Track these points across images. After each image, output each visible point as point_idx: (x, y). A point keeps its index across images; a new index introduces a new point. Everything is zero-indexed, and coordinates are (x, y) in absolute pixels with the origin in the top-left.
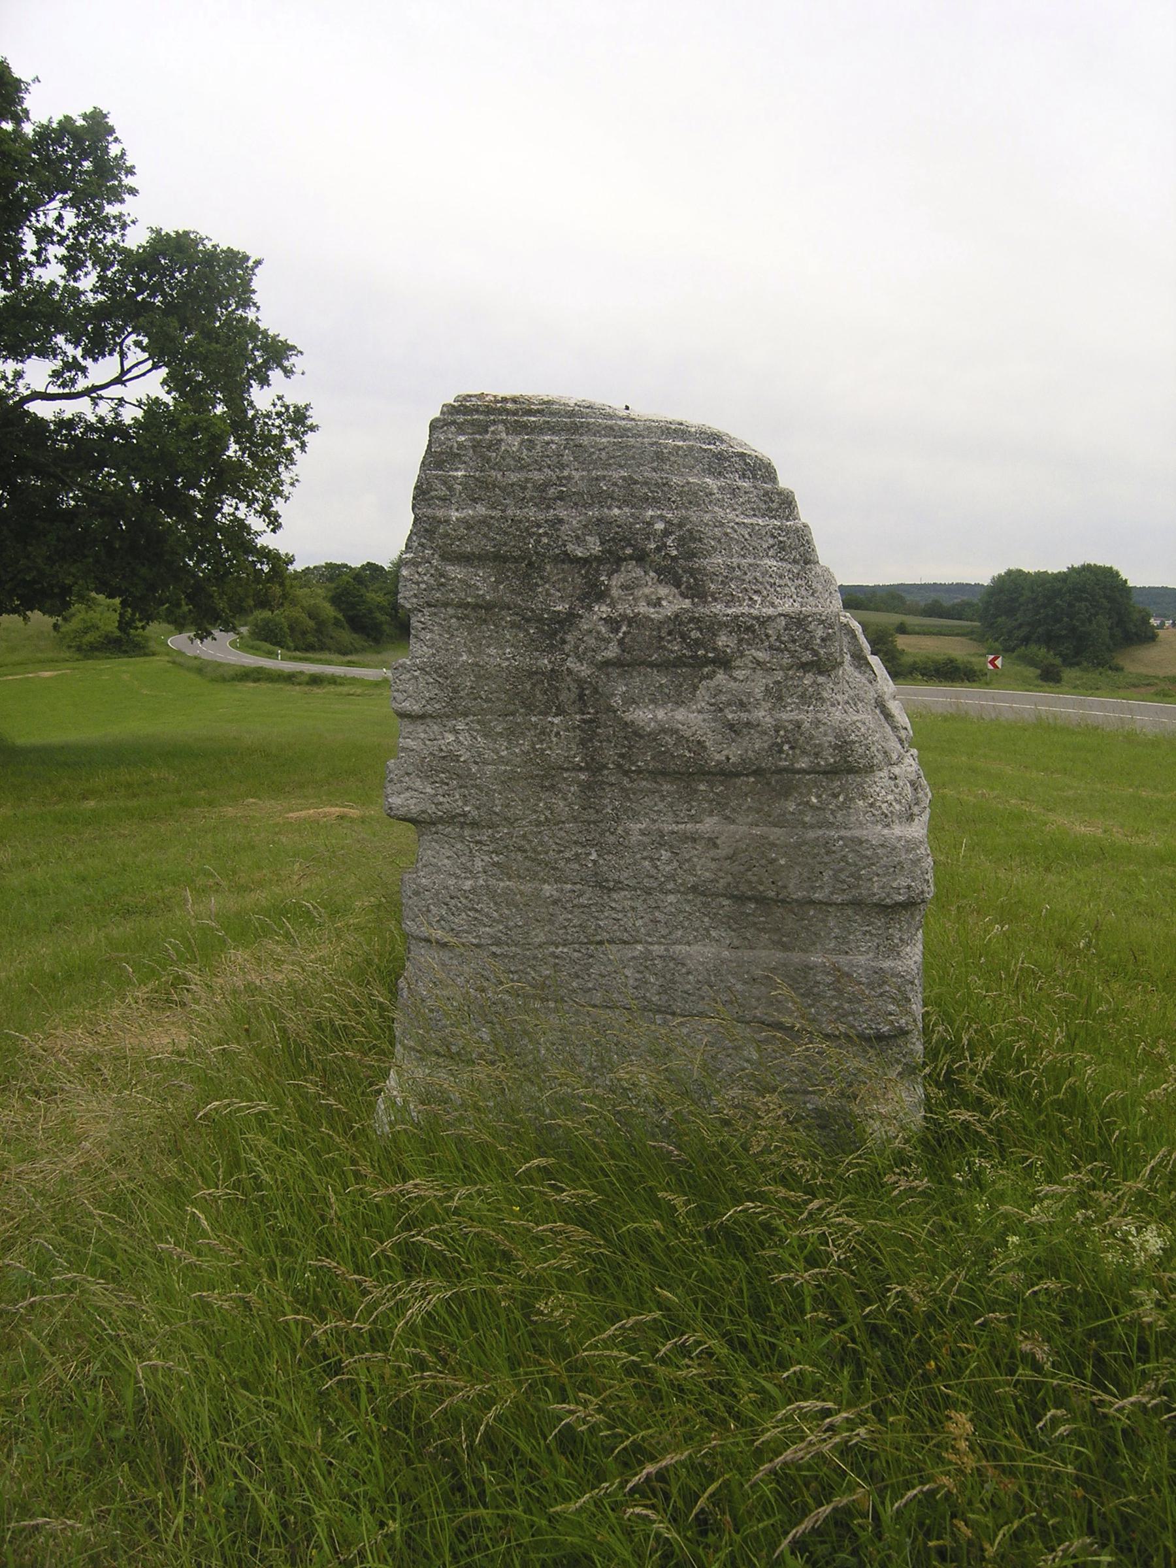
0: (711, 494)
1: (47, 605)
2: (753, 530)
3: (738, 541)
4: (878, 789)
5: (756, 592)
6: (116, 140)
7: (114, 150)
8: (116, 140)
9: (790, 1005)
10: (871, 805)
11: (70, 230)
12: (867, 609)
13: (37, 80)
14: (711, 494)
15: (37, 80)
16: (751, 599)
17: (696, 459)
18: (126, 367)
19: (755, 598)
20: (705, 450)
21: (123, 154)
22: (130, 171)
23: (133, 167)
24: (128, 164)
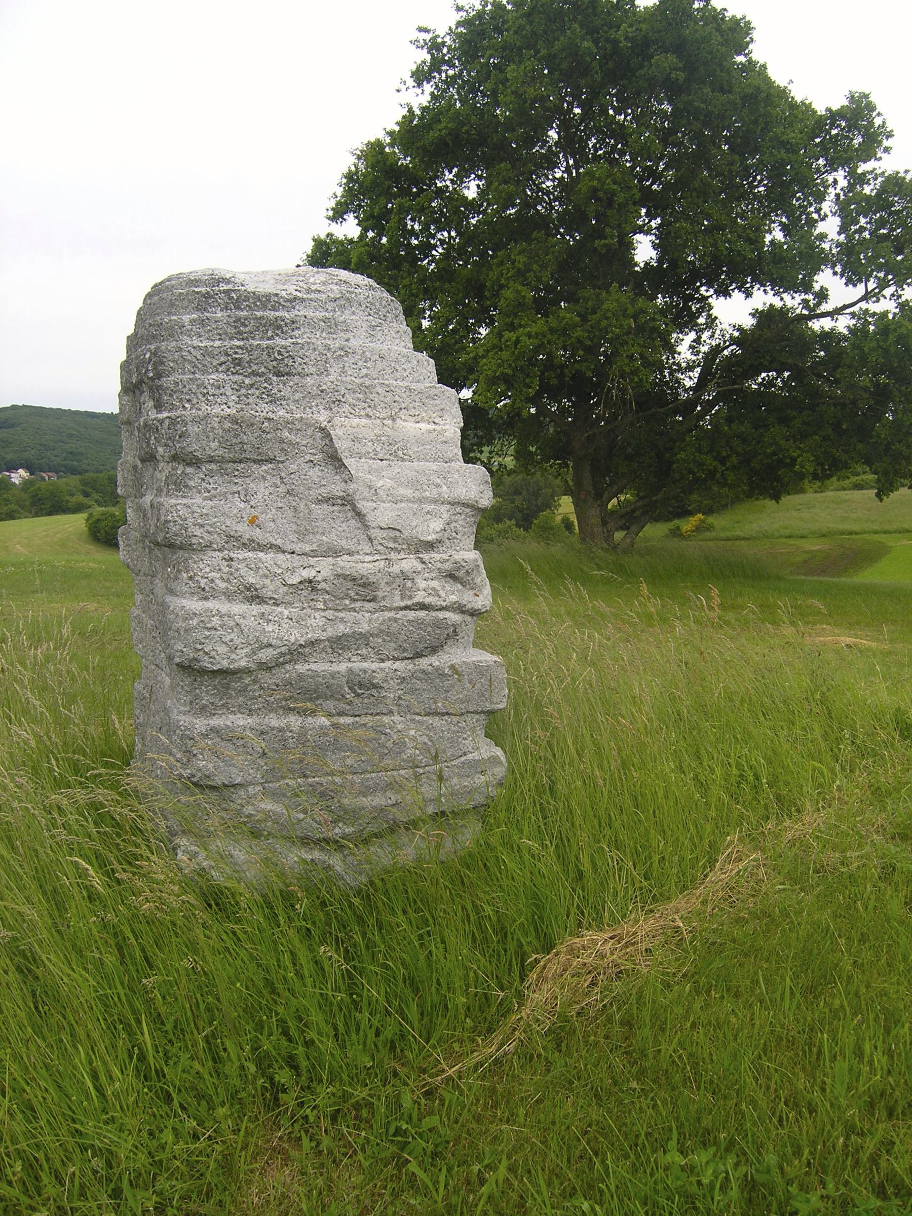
0: (184, 326)
1: (126, 398)
2: (206, 352)
3: (190, 362)
4: (202, 566)
5: (189, 401)
6: (879, 114)
7: (878, 122)
8: (879, 114)
9: (841, 898)
10: (191, 578)
11: (842, 189)
12: (867, 489)
13: (791, 81)
14: (184, 326)
15: (791, 81)
16: (184, 406)
17: (189, 301)
18: (869, 290)
19: (187, 405)
20: (197, 293)
21: (884, 122)
22: (890, 135)
23: (892, 131)
24: (888, 130)
